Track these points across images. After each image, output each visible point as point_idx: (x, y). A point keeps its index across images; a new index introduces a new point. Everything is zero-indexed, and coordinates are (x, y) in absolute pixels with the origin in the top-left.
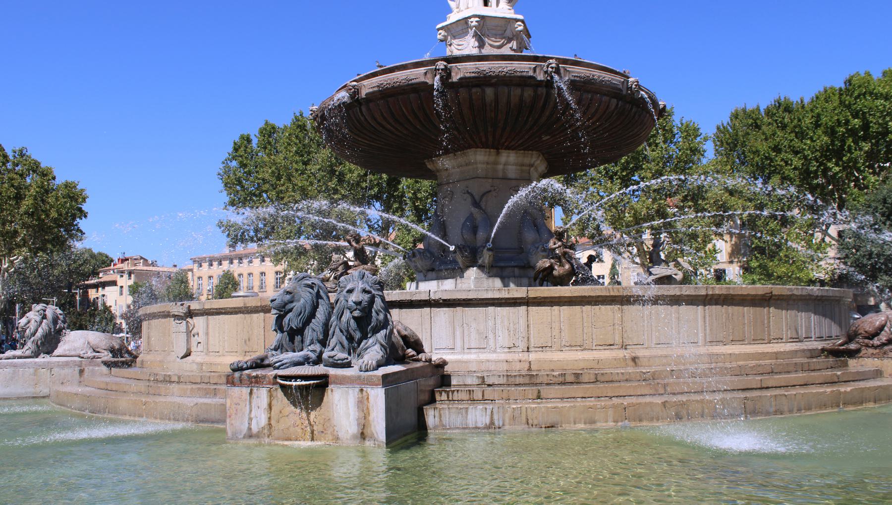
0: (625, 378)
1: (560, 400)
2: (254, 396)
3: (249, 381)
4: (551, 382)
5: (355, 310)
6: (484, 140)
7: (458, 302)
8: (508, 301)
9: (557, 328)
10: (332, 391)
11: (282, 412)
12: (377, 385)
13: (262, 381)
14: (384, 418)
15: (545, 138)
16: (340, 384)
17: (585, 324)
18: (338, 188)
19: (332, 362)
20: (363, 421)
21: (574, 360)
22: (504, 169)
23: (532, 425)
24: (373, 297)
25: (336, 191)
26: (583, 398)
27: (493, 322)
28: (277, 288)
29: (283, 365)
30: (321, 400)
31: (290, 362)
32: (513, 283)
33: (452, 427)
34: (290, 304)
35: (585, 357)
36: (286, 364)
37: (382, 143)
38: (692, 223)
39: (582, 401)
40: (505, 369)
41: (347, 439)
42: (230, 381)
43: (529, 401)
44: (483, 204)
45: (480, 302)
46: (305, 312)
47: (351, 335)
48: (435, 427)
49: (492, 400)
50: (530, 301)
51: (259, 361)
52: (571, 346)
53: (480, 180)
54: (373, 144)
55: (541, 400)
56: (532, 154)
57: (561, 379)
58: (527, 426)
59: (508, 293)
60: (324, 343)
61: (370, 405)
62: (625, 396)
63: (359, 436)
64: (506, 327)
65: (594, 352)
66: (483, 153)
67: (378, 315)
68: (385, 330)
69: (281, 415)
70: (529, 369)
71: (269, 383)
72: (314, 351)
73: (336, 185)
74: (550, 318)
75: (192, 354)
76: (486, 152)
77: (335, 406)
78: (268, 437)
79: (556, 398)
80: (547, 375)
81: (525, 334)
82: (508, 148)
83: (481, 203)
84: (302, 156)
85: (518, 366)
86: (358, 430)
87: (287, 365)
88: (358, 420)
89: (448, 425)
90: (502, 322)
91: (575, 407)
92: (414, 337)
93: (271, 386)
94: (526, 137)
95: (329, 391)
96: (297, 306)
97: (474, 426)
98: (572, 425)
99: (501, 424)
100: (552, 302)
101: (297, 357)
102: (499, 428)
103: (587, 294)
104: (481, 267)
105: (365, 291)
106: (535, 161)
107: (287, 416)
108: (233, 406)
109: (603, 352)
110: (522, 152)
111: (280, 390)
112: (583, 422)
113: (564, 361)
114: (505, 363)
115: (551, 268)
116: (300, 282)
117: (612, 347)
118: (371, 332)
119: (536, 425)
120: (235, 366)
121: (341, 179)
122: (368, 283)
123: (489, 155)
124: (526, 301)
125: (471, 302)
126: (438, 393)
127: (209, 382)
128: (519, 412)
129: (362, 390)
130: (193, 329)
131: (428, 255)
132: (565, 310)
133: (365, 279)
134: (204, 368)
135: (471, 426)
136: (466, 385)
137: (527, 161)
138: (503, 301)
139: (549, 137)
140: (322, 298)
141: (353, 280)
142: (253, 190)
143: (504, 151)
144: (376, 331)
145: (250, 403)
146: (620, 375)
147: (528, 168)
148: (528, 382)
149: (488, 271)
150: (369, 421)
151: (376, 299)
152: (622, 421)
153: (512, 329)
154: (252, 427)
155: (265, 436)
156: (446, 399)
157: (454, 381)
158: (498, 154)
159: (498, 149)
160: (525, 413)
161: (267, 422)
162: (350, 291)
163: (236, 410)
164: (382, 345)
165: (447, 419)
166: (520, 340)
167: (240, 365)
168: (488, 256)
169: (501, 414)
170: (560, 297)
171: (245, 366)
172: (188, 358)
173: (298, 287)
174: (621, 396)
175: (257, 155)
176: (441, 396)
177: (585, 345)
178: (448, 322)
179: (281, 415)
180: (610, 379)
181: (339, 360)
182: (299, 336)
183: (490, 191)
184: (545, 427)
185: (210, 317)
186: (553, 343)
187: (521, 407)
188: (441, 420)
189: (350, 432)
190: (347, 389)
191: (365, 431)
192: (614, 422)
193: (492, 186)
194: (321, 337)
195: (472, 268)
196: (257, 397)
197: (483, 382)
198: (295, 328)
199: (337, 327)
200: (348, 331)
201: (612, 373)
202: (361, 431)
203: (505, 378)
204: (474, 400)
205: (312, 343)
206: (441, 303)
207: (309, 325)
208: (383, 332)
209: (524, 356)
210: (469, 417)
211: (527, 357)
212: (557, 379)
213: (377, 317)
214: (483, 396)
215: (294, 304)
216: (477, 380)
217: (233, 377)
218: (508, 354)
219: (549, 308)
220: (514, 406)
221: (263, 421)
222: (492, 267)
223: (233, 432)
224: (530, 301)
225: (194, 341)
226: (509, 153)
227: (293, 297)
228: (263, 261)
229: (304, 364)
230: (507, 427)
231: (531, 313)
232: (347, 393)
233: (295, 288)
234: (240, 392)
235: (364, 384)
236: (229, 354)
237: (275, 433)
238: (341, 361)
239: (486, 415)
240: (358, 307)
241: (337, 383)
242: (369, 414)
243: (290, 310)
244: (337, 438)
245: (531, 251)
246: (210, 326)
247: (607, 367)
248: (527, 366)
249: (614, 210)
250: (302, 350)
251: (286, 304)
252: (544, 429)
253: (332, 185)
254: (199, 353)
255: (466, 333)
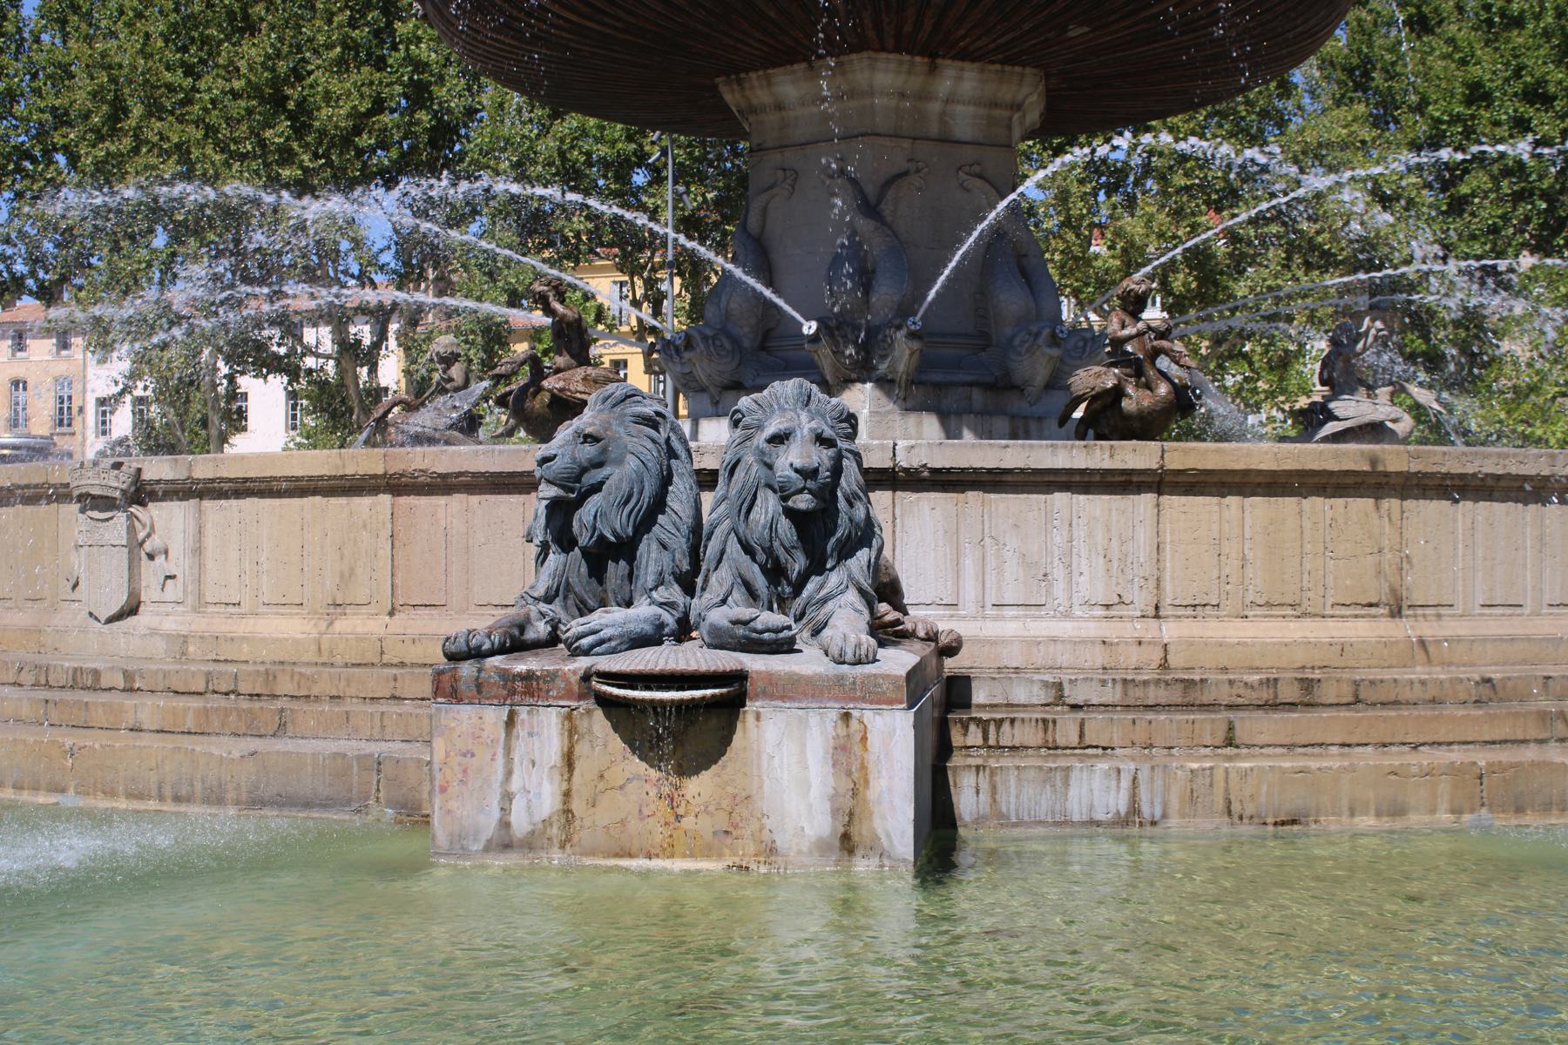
0: (1428, 696)
1: (1284, 751)
2: (520, 731)
3: (504, 686)
4: (1240, 701)
5: (800, 491)
6: (908, 28)
7: (973, 477)
8: (1109, 479)
9: (1234, 555)
10: (758, 717)
11: (606, 774)
12: (890, 702)
13: (544, 687)
14: (911, 795)
15: (1075, 32)
16: (783, 698)
17: (1308, 547)
18: (295, 145)
19: (745, 637)
20: (848, 803)
21: (1280, 643)
22: (943, 114)
23: (1241, 818)
24: (838, 458)
25: (287, 155)
26: (1343, 745)
27: (1065, 533)
28: (61, 423)
29: (601, 642)
30: (726, 741)
31: (621, 636)
32: (969, 428)
33: (1026, 818)
34: (594, 472)
35: (1308, 634)
36: (610, 639)
37: (619, 25)
38: (1279, 282)
39: (1342, 755)
40: (1099, 662)
41: (800, 852)
42: (447, 690)
43: (1204, 751)
44: (886, 209)
45: (1032, 478)
46: (641, 493)
47: (777, 560)
48: (979, 820)
49: (1104, 748)
50: (1168, 479)
51: (516, 632)
52: (1269, 604)
53: (881, 140)
54: (590, 24)
55: (1236, 751)
56: (1022, 75)
57: (1265, 695)
58: (1226, 819)
59: (1112, 456)
60: (688, 584)
61: (871, 758)
62: (1450, 744)
63: (837, 843)
64: (1100, 548)
65: (1330, 623)
66: (892, 66)
67: (851, 505)
68: (866, 550)
69: (601, 786)
70: (1164, 666)
71: (568, 695)
72: (668, 605)
73: (288, 139)
74: (1215, 527)
75: (142, 608)
76: (901, 63)
77: (765, 757)
78: (562, 847)
79: (1276, 746)
80: (1231, 682)
81: (1148, 570)
82: (964, 56)
83: (883, 206)
84: (184, 49)
85: (1133, 657)
86: (834, 829)
87: (613, 644)
88: (833, 798)
89: (1013, 814)
90: (1090, 535)
91: (1352, 769)
92: (890, 571)
93: (574, 704)
94: (1026, 27)
95: (750, 718)
96: (618, 477)
97: (1085, 818)
98: (1345, 819)
99: (1158, 813)
100: (1223, 484)
101: (637, 620)
102: (1153, 823)
103: (1315, 466)
104: (885, 383)
105: (821, 440)
106: (1027, 96)
107: (621, 788)
108: (456, 760)
109: (1351, 624)
110: (998, 67)
111: (599, 714)
112: (1373, 812)
113: (1253, 645)
114: (1099, 648)
115: (1118, 392)
116: (617, 409)
117: (1373, 610)
118: (835, 554)
119: (1252, 817)
120: (461, 645)
121: (301, 120)
122: (823, 417)
123: (909, 73)
124: (1157, 479)
125: (1009, 478)
126: (959, 725)
127: (233, 692)
128: (1208, 780)
129: (846, 717)
130: (149, 536)
131: (728, 345)
132: (1258, 507)
133: (813, 406)
134: (191, 649)
135: (1076, 818)
136: (1012, 705)
137: (1006, 93)
138: (1097, 478)
139: (1086, 29)
140: (676, 457)
141: (781, 408)
142: (23, 143)
143: (948, 62)
144: (846, 551)
145: (508, 750)
146: (1417, 686)
147: (1006, 113)
148: (1179, 701)
149: (902, 394)
150: (865, 800)
151: (845, 462)
152: (1472, 811)
153: (1115, 554)
154: (514, 819)
155: (551, 845)
156: (980, 742)
157: (979, 696)
158: (933, 69)
159: (933, 56)
160: (1222, 784)
161: (559, 806)
162: (779, 439)
163: (465, 771)
164: (862, 592)
165: (1012, 799)
166: (1136, 586)
167: (474, 643)
168: (907, 352)
169: (1159, 782)
170: (1246, 472)
171: (487, 646)
172: (132, 620)
173: (614, 423)
174: (1440, 744)
175: (37, 40)
176: (965, 735)
177: (1306, 603)
178: (941, 532)
179: (601, 786)
180: (1392, 698)
181: (768, 630)
182: (622, 563)
183: (906, 173)
184: (1276, 824)
185: (207, 504)
186: (1224, 596)
187: (1211, 768)
188: (995, 801)
189: (808, 831)
190: (801, 712)
191: (854, 831)
192: (1453, 812)
193: (911, 160)
194: (686, 567)
195: (859, 385)
196: (531, 734)
197: (1059, 699)
198: (612, 539)
199: (733, 538)
200: (769, 551)
201: (1395, 680)
202: (841, 830)
203: (1119, 687)
204: (1056, 748)
205: (660, 582)
206: (924, 480)
207: (648, 531)
208: (863, 555)
209: (1148, 629)
210: (1073, 792)
211: (1156, 634)
212: (1254, 695)
213: (847, 516)
214: (1081, 735)
215: (606, 471)
216: (1042, 693)
217: (454, 676)
218: (1104, 624)
219: (1215, 500)
220: (1195, 766)
221: (547, 800)
222: (914, 381)
223: (451, 835)
224: (1168, 479)
225: (151, 573)
226: (962, 69)
227: (604, 451)
228: (64, 345)
229: (660, 643)
230: (1174, 821)
231: (1167, 514)
232: (804, 723)
233: (607, 426)
234: (475, 720)
235: (854, 699)
236: (275, 609)
237: (583, 836)
238: (773, 636)
239: (1118, 787)
240: (810, 484)
241: (772, 697)
242: (867, 782)
243: (597, 488)
244: (772, 850)
245: (1017, 342)
246: (210, 530)
247: (1363, 663)
248: (1157, 656)
249: (1070, 236)
250: (629, 604)
251: (584, 470)
252: (1271, 828)
253: (277, 134)
254: (169, 608)
255: (991, 562)
